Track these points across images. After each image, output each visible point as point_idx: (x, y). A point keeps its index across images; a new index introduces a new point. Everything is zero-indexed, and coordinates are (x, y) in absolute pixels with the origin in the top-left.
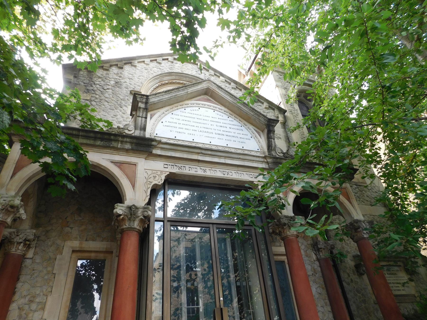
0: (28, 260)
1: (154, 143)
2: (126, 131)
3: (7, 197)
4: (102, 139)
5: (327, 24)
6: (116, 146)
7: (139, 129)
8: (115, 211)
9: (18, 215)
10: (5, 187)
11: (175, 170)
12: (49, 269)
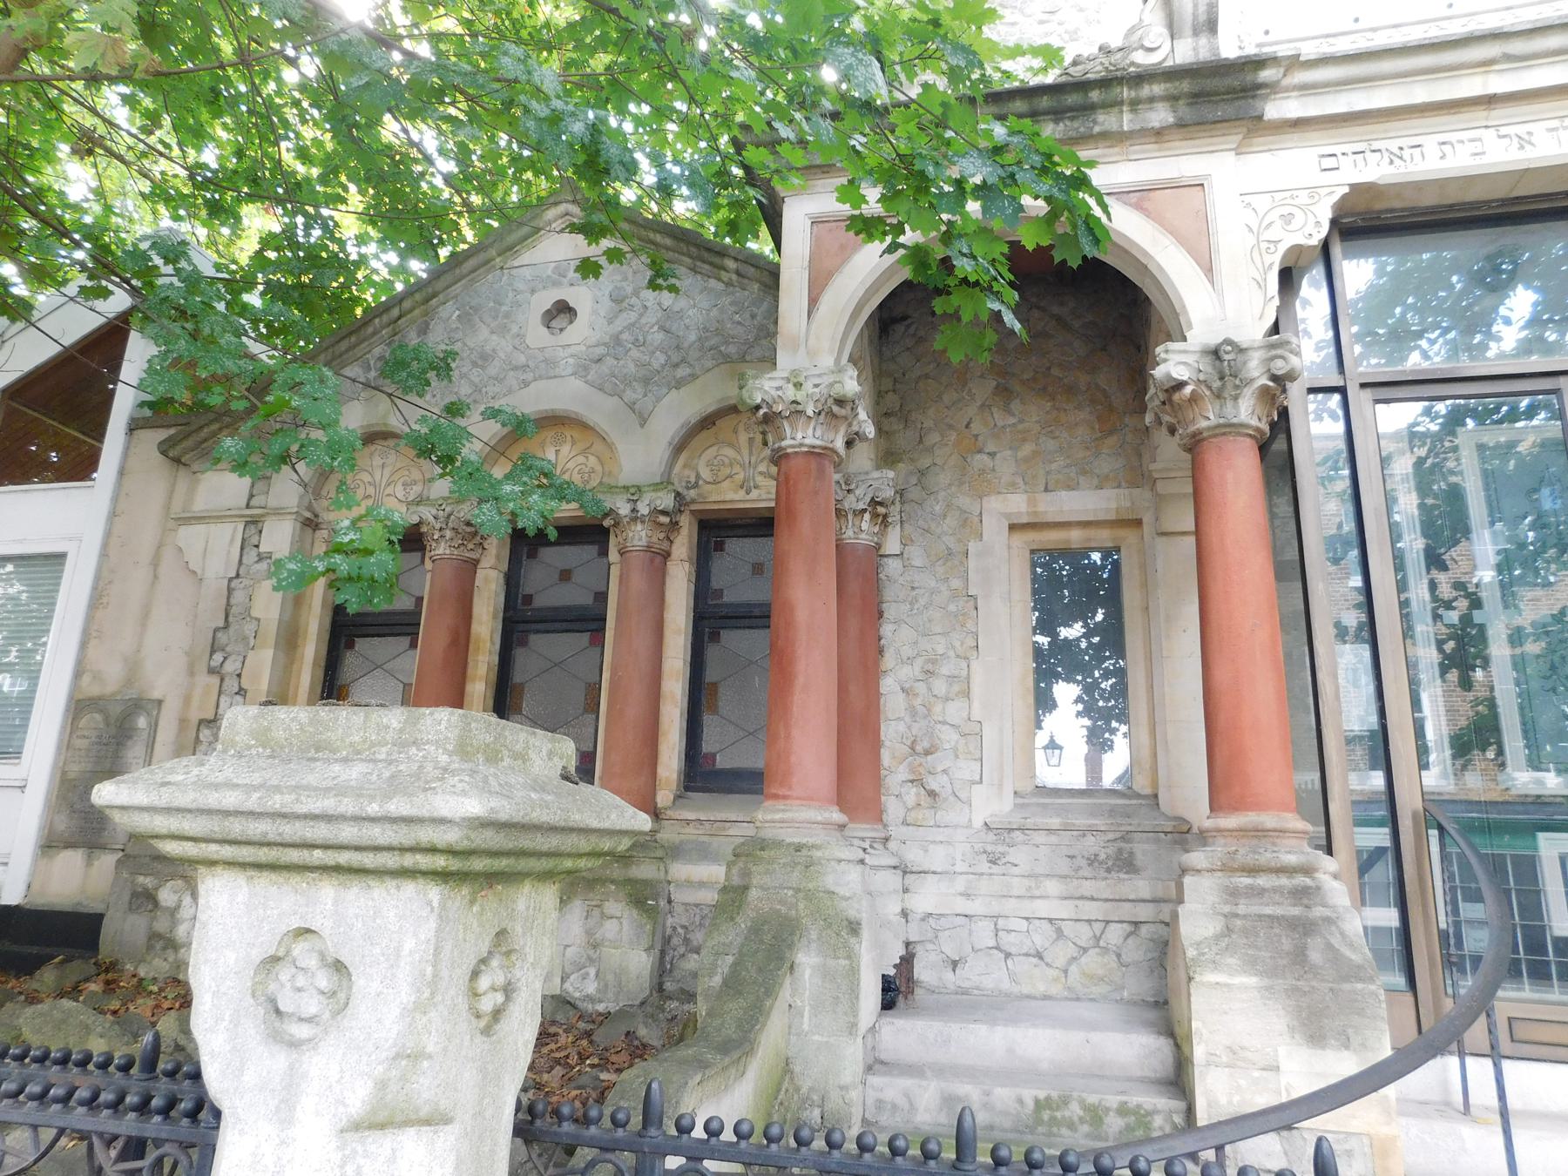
0: (890, 561)
1: (1266, 75)
2: (1141, 58)
3: (819, 376)
4: (1057, 114)
6: (1115, 128)
7: (1188, 30)
8: (1158, 372)
9: (855, 428)
10: (802, 348)
11: (1375, 170)
12: (956, 583)
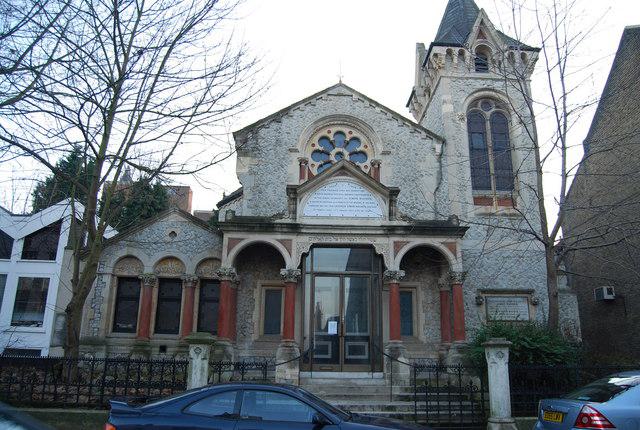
5: (555, 244)
